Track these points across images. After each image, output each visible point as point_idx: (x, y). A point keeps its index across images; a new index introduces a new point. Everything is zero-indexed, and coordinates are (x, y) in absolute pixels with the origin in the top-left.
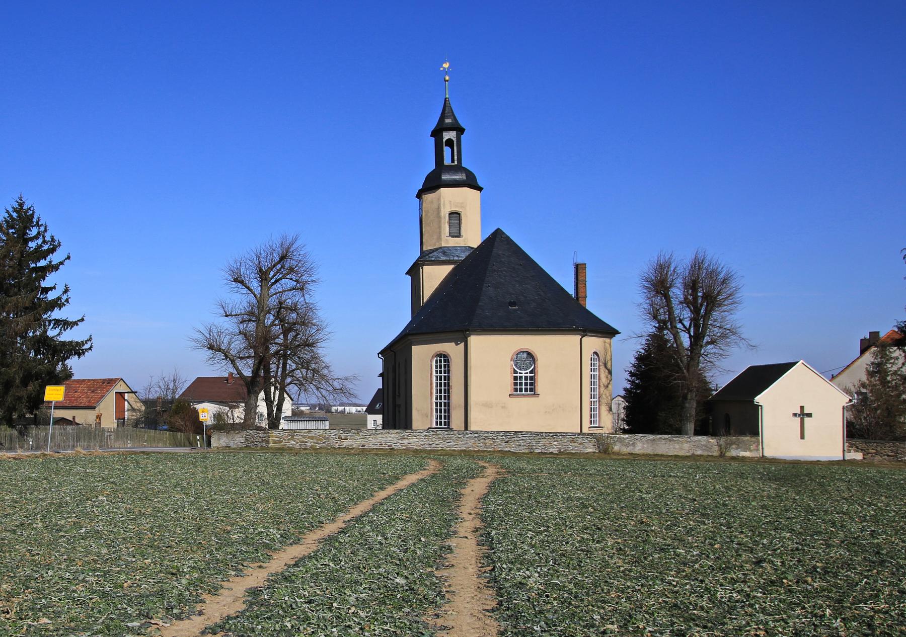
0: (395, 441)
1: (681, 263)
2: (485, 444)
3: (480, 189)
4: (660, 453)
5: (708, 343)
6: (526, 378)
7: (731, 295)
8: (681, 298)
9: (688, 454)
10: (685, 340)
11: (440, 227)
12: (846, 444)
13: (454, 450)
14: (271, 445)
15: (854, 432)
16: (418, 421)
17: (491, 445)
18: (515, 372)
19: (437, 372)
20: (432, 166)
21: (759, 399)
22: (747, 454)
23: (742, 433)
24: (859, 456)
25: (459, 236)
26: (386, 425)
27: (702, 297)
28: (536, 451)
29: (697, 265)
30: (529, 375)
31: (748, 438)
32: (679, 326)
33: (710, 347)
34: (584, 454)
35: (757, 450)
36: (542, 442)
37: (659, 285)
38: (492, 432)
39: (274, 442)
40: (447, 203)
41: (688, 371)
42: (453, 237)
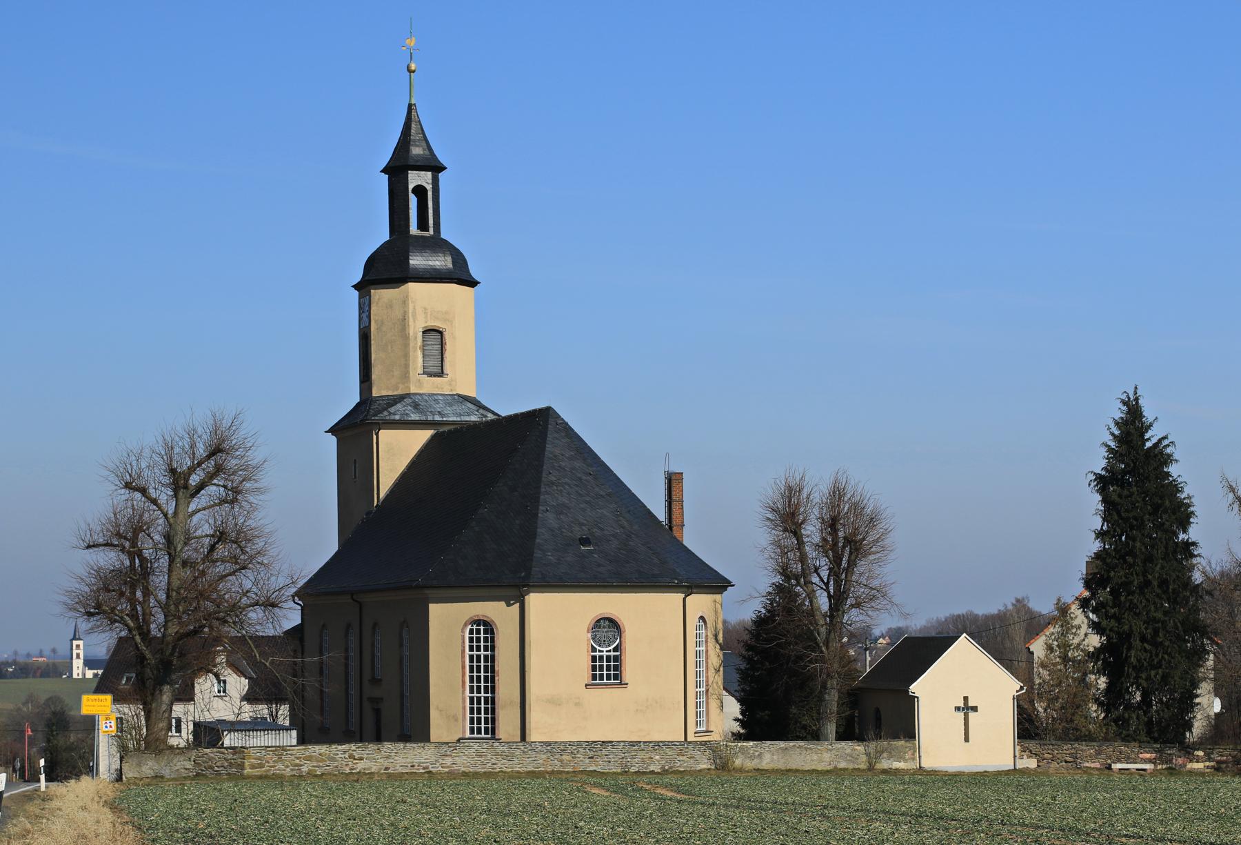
0: (433, 759)
1: (817, 489)
2: (561, 761)
4: (794, 767)
5: (852, 606)
6: (609, 658)
7: (877, 541)
8: (817, 539)
9: (829, 768)
10: (823, 602)
11: (406, 356)
12: (1018, 748)
13: (518, 772)
14: (247, 771)
15: (1028, 728)
16: (439, 728)
17: (569, 763)
18: (594, 650)
19: (471, 649)
20: (381, 234)
21: (915, 688)
22: (901, 765)
23: (896, 737)
24: (1032, 763)
25: (441, 374)
26: (302, 741)
27: (845, 538)
28: (632, 770)
29: (837, 494)
30: (612, 654)
31: (902, 743)
32: (815, 579)
33: (854, 611)
34: (696, 771)
35: (914, 759)
36: (641, 755)
37: (788, 518)
38: (571, 744)
39: (253, 767)
40: (419, 311)
41: (827, 648)
42: (430, 375)
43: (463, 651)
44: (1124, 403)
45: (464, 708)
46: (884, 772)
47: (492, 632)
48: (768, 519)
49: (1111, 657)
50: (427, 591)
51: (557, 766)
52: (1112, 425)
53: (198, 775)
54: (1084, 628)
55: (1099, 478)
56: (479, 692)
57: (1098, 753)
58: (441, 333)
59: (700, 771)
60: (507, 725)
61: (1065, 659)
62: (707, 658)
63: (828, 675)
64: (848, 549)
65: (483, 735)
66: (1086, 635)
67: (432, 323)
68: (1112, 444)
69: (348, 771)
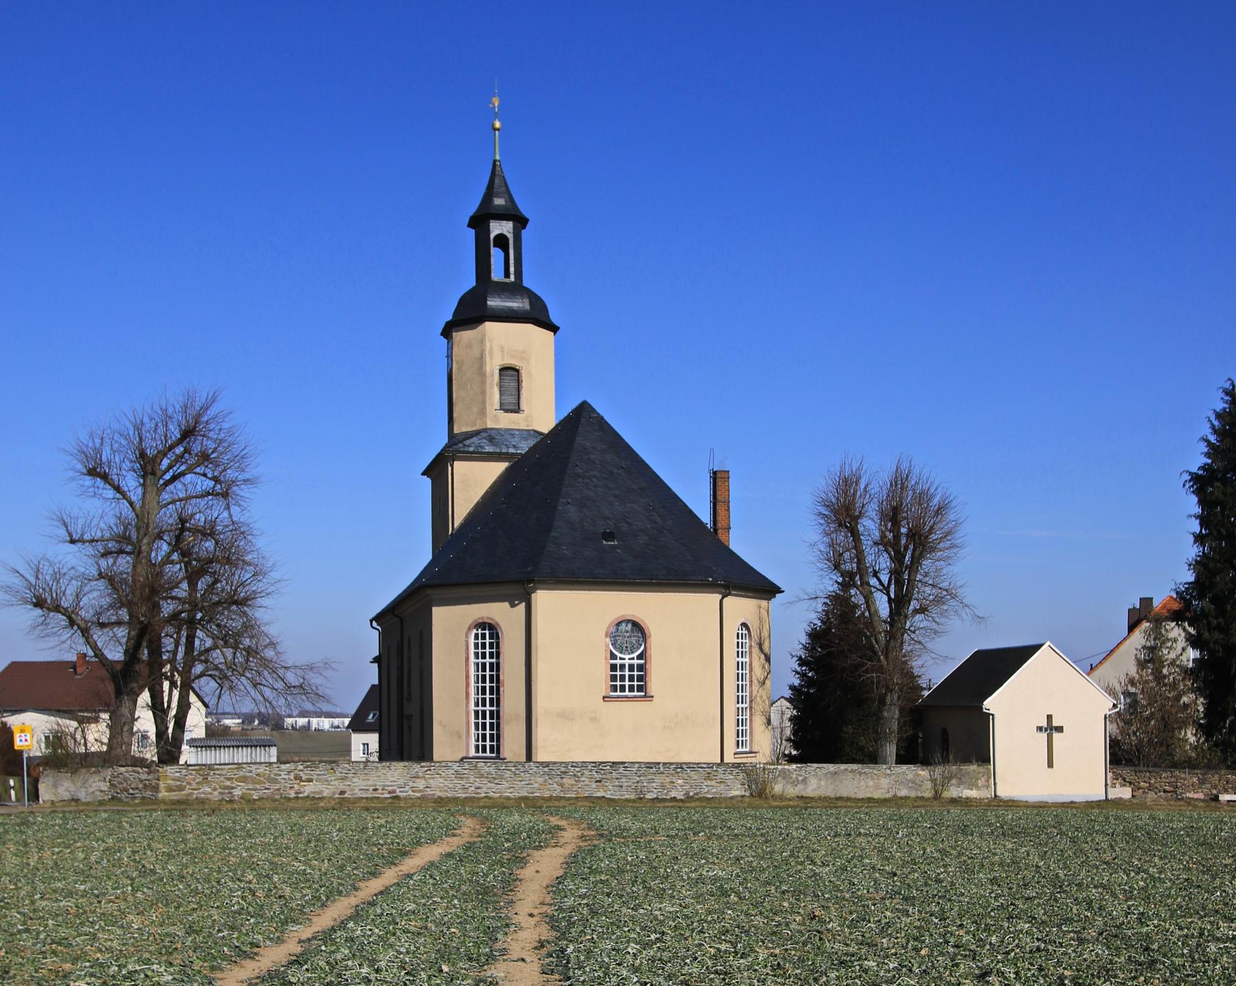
0: (401, 782)
1: (876, 481)
2: (562, 785)
3: (554, 328)
4: (845, 794)
5: (916, 611)
6: (631, 668)
8: (876, 535)
9: (887, 796)
10: (882, 606)
11: (483, 392)
12: (1110, 775)
14: (163, 794)
15: (1120, 756)
17: (572, 787)
18: (613, 657)
19: (477, 655)
20: (470, 282)
21: (990, 704)
23: (966, 760)
24: (1125, 793)
25: (517, 409)
28: (649, 796)
29: (899, 482)
30: (636, 662)
31: (973, 767)
32: (873, 581)
33: (919, 617)
34: (726, 799)
35: (988, 787)
36: (659, 779)
37: (843, 514)
38: (574, 765)
39: (170, 789)
40: (496, 349)
41: (887, 657)
42: (507, 411)
43: (467, 659)
44: (1227, 392)
45: (468, 723)
46: (954, 801)
47: (498, 637)
48: (820, 514)
49: (1211, 675)
50: (429, 592)
51: (556, 791)
52: (1213, 418)
53: (113, 798)
54: (1181, 643)
55: (1195, 478)
56: (484, 705)
57: (1202, 782)
58: (517, 371)
59: (732, 798)
60: (513, 746)
61: (1159, 677)
62: (751, 670)
63: (887, 688)
64: (911, 547)
65: (488, 754)
66: (1184, 649)
67: (509, 361)
68: (1212, 439)
69: (293, 795)
